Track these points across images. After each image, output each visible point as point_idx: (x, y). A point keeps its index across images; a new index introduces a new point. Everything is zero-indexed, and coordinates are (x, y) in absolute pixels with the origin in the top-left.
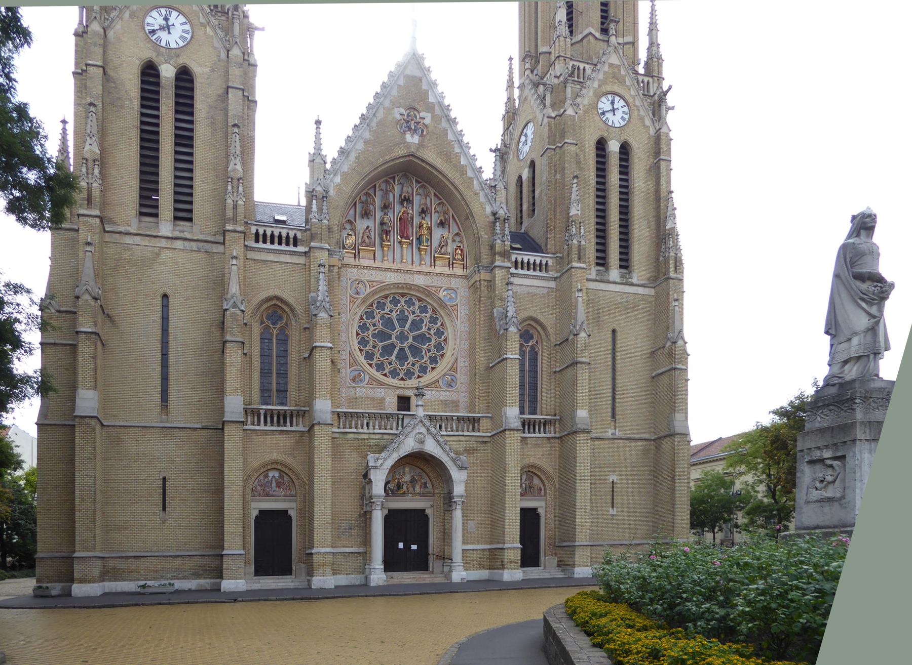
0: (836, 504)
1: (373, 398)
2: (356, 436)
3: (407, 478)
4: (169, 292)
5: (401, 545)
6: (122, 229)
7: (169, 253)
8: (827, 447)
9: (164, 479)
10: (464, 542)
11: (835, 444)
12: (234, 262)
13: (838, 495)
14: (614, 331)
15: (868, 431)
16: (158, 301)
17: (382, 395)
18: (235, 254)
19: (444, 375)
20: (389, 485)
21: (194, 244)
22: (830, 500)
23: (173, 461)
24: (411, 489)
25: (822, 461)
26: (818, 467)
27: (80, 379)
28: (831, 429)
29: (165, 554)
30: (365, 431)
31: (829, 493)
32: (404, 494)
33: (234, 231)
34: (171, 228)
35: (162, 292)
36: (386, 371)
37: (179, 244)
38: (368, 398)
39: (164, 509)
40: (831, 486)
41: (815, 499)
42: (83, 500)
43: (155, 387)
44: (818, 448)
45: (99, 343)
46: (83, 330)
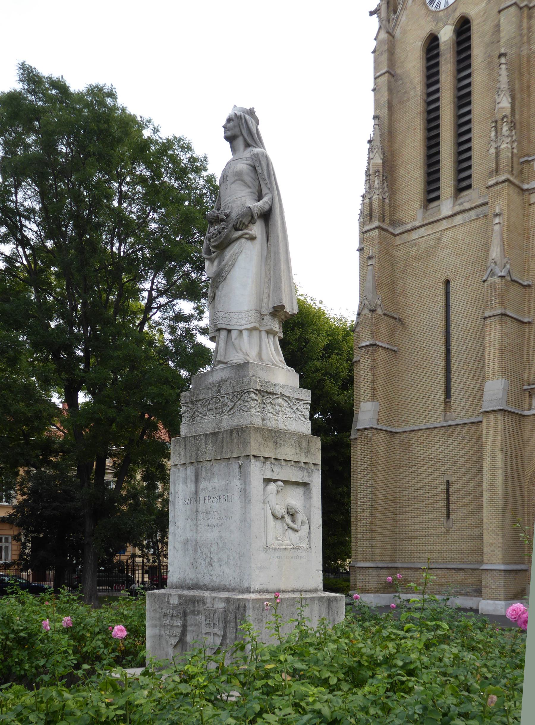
4: (450, 276)
6: (409, 227)
7: (449, 233)
9: (448, 483)
12: (497, 220)
14: (447, 282)
15: (182, 453)
16: (441, 289)
18: (497, 211)
21: (473, 213)
23: (455, 463)
27: (362, 393)
29: (449, 566)
33: (497, 184)
34: (451, 205)
35: (443, 278)
37: (459, 219)
39: (448, 517)
42: (363, 511)
43: (439, 384)
46: (363, 344)
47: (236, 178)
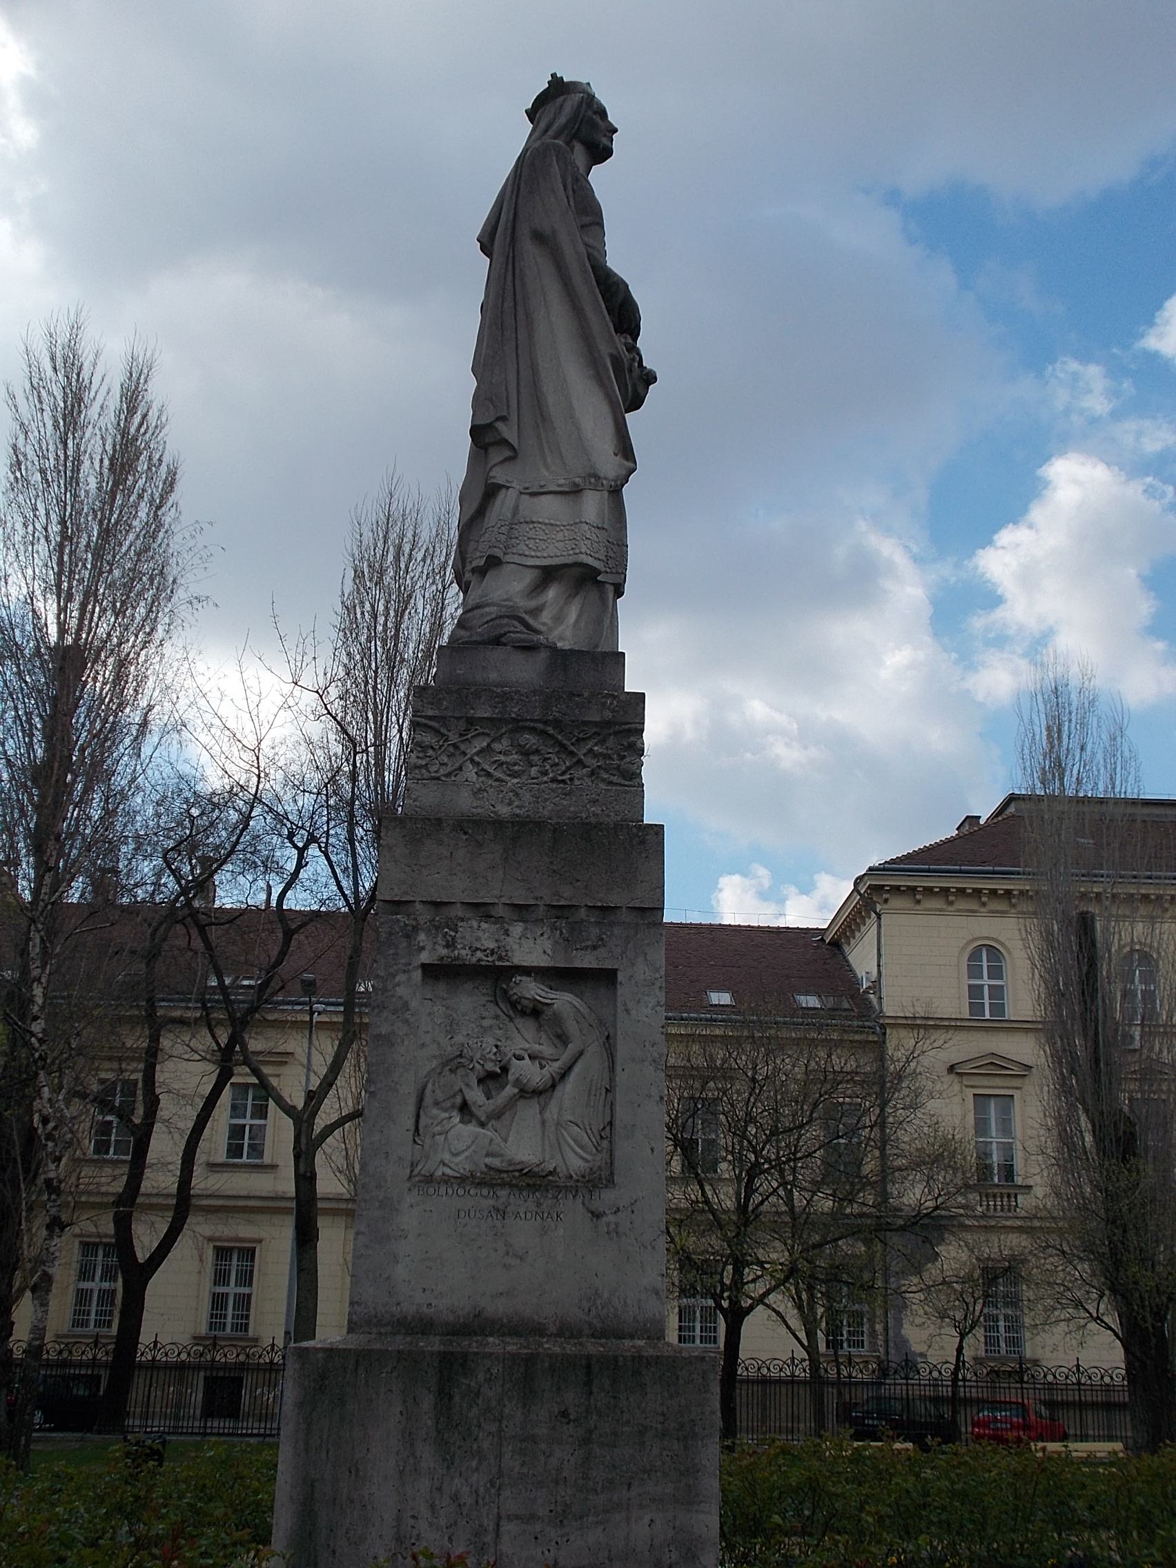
0: (573, 1209)
5: (721, 998)
8: (521, 911)
10: (114, 1291)
11: (560, 911)
13: (575, 1162)
22: (533, 1181)
25: (496, 976)
26: (469, 1002)
28: (516, 833)
31: (524, 1143)
40: (528, 1112)
41: (461, 1165)
44: (482, 910)
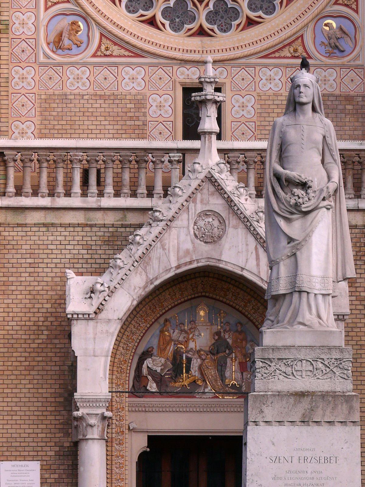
1: (114, 97)
2: (51, 218)
3: (202, 339)
17: (138, 86)
19: (321, 17)
20: (148, 362)
24: (212, 372)
30: (76, 201)
32: (189, 392)
36: (202, 20)
38: (97, 96)
45: (322, 12)
47: (314, 145)
